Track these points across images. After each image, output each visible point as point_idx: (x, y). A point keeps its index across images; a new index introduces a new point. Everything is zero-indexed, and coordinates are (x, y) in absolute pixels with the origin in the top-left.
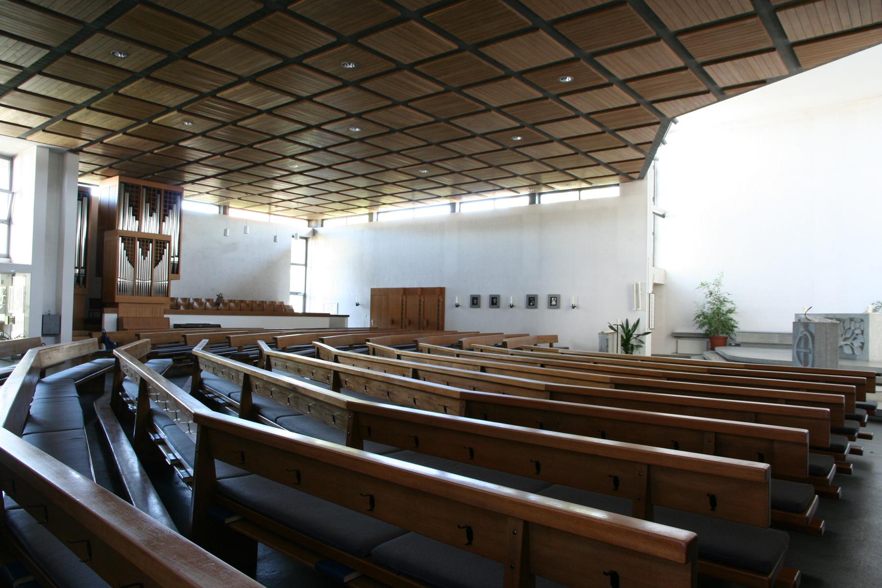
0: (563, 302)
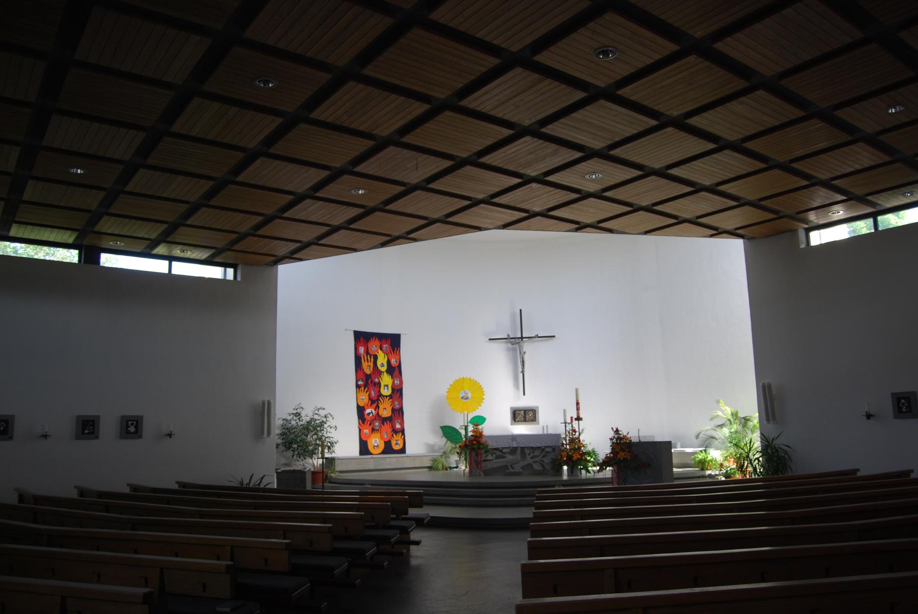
0: (148, 428)
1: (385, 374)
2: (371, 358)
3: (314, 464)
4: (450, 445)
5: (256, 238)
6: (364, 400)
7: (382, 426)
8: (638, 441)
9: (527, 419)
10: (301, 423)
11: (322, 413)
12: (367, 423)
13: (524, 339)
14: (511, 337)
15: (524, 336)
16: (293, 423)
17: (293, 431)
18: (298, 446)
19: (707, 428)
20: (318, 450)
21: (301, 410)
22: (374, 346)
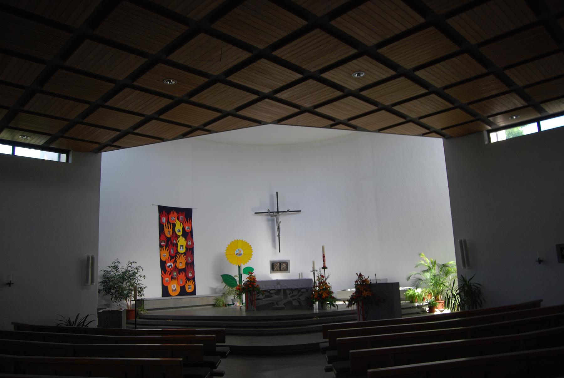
1: (181, 237)
2: (171, 226)
3: (128, 305)
4: (227, 288)
5: (83, 126)
6: (166, 256)
7: (179, 275)
8: (375, 282)
9: (282, 269)
10: (118, 273)
11: (134, 266)
12: (168, 273)
13: (279, 213)
14: (270, 211)
15: (279, 211)
16: (112, 273)
17: (112, 280)
18: (116, 291)
19: (414, 273)
20: (131, 294)
21: (118, 263)
22: (173, 217)
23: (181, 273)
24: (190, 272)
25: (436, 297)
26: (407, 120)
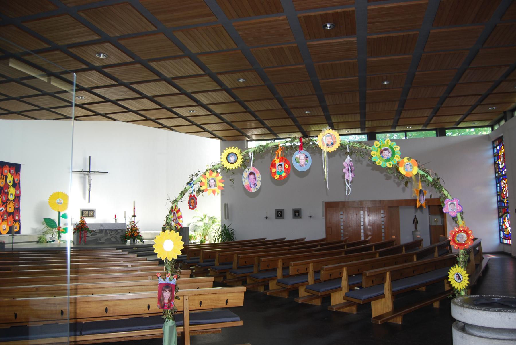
1: (11, 187)
9: (90, 215)
13: (91, 173)
14: (84, 171)
15: (91, 171)
23: (10, 216)
24: (17, 215)
25: (204, 237)
26: (205, 131)
